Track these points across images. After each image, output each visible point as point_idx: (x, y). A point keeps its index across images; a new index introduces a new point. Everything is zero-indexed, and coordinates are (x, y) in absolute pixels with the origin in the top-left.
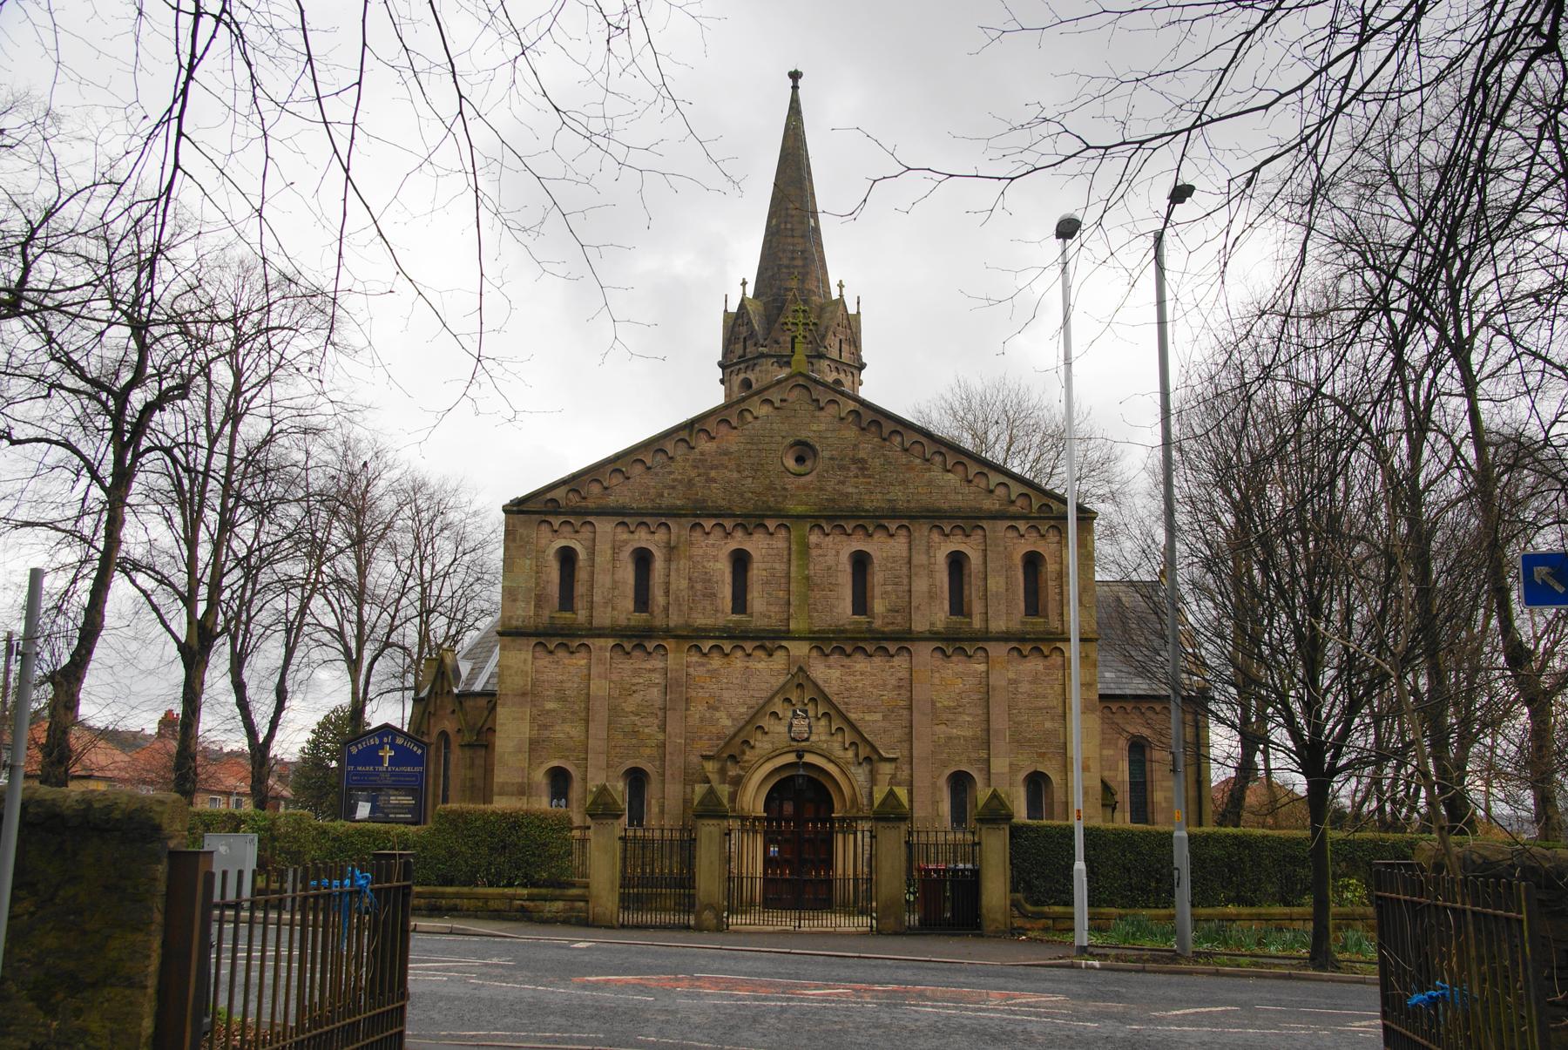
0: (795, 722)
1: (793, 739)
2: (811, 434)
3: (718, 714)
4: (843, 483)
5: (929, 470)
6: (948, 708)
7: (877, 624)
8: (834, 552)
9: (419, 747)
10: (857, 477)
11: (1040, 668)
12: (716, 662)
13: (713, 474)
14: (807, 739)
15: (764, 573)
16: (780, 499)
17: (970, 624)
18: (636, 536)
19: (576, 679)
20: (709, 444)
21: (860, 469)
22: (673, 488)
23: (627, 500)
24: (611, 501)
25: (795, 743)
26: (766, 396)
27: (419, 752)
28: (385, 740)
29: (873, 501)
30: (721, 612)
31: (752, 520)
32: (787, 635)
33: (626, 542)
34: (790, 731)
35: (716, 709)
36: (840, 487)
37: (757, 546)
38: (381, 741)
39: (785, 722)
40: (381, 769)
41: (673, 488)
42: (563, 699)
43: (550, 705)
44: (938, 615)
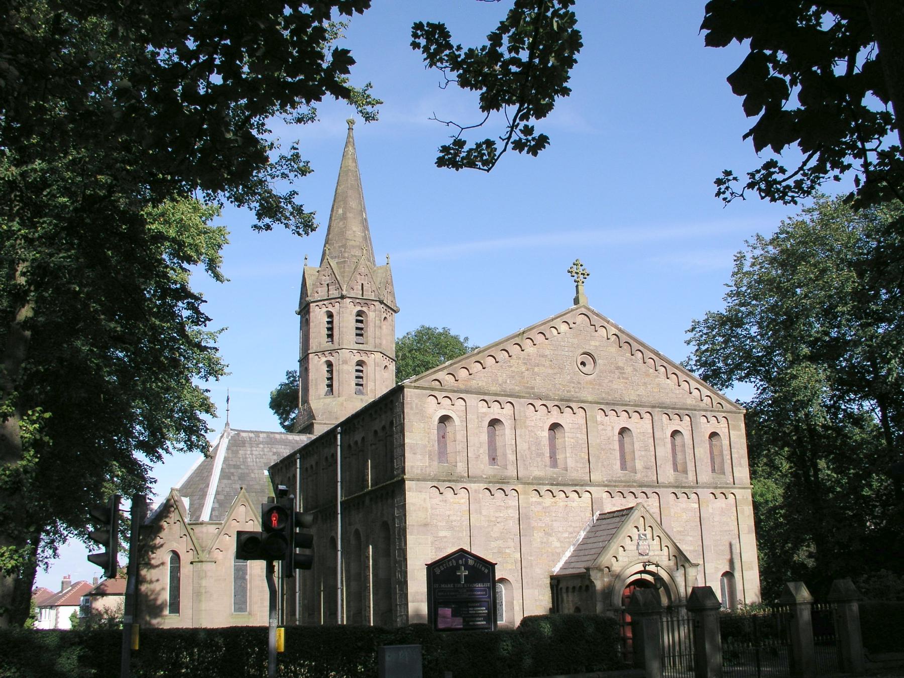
0: (641, 543)
1: (641, 554)
2: (591, 348)
3: (551, 539)
4: (611, 381)
5: (657, 376)
6: (680, 532)
7: (638, 476)
8: (610, 428)
9: (486, 567)
10: (619, 378)
11: (724, 506)
12: (548, 500)
13: (536, 369)
14: (647, 555)
15: (572, 440)
16: (577, 390)
17: (687, 478)
18: (491, 410)
19: (459, 513)
20: (532, 348)
21: (621, 373)
22: (513, 377)
23: (484, 384)
24: (474, 384)
25: (641, 557)
26: (565, 318)
27: (486, 571)
28: (460, 562)
29: (631, 396)
30: (538, 469)
31: (565, 403)
32: (590, 483)
33: (485, 414)
34: (638, 549)
35: (550, 535)
36: (610, 384)
37: (566, 419)
38: (457, 562)
39: (635, 542)
40: (459, 585)
41: (513, 377)
42: (451, 528)
43: (442, 534)
44: (667, 474)
